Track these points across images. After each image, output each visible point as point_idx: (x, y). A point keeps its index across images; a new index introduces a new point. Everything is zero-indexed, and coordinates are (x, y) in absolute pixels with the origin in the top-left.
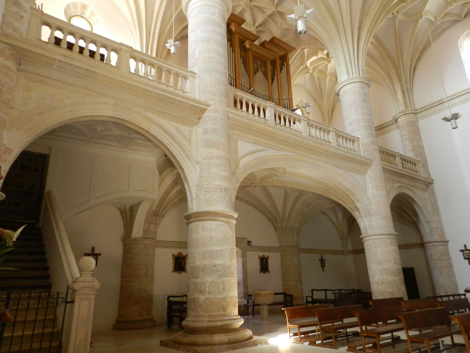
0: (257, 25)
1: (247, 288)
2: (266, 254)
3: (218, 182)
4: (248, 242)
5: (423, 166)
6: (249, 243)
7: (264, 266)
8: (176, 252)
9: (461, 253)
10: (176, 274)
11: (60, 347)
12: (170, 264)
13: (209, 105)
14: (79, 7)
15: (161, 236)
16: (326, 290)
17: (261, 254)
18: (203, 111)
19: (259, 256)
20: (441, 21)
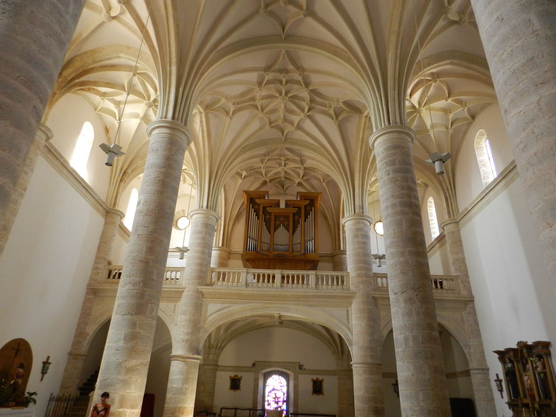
0: (301, 176)
1: (297, 407)
2: (321, 378)
3: (182, 337)
4: (300, 366)
5: (462, 281)
6: (301, 367)
7: (317, 387)
8: (232, 374)
9: (393, 386)
10: (232, 392)
11: (85, 415)
12: (228, 383)
13: (185, 288)
14: (181, 212)
15: (222, 362)
16: (236, 409)
17: (315, 377)
18: (182, 292)
19: (312, 379)
20: (453, 128)
